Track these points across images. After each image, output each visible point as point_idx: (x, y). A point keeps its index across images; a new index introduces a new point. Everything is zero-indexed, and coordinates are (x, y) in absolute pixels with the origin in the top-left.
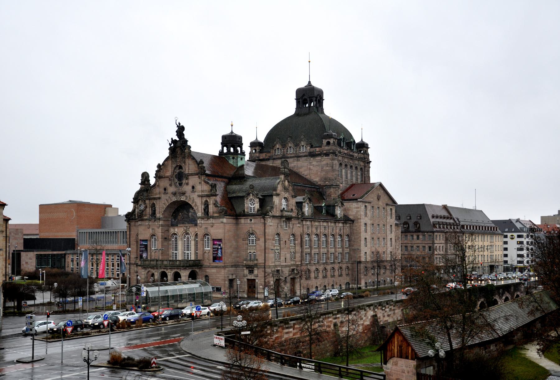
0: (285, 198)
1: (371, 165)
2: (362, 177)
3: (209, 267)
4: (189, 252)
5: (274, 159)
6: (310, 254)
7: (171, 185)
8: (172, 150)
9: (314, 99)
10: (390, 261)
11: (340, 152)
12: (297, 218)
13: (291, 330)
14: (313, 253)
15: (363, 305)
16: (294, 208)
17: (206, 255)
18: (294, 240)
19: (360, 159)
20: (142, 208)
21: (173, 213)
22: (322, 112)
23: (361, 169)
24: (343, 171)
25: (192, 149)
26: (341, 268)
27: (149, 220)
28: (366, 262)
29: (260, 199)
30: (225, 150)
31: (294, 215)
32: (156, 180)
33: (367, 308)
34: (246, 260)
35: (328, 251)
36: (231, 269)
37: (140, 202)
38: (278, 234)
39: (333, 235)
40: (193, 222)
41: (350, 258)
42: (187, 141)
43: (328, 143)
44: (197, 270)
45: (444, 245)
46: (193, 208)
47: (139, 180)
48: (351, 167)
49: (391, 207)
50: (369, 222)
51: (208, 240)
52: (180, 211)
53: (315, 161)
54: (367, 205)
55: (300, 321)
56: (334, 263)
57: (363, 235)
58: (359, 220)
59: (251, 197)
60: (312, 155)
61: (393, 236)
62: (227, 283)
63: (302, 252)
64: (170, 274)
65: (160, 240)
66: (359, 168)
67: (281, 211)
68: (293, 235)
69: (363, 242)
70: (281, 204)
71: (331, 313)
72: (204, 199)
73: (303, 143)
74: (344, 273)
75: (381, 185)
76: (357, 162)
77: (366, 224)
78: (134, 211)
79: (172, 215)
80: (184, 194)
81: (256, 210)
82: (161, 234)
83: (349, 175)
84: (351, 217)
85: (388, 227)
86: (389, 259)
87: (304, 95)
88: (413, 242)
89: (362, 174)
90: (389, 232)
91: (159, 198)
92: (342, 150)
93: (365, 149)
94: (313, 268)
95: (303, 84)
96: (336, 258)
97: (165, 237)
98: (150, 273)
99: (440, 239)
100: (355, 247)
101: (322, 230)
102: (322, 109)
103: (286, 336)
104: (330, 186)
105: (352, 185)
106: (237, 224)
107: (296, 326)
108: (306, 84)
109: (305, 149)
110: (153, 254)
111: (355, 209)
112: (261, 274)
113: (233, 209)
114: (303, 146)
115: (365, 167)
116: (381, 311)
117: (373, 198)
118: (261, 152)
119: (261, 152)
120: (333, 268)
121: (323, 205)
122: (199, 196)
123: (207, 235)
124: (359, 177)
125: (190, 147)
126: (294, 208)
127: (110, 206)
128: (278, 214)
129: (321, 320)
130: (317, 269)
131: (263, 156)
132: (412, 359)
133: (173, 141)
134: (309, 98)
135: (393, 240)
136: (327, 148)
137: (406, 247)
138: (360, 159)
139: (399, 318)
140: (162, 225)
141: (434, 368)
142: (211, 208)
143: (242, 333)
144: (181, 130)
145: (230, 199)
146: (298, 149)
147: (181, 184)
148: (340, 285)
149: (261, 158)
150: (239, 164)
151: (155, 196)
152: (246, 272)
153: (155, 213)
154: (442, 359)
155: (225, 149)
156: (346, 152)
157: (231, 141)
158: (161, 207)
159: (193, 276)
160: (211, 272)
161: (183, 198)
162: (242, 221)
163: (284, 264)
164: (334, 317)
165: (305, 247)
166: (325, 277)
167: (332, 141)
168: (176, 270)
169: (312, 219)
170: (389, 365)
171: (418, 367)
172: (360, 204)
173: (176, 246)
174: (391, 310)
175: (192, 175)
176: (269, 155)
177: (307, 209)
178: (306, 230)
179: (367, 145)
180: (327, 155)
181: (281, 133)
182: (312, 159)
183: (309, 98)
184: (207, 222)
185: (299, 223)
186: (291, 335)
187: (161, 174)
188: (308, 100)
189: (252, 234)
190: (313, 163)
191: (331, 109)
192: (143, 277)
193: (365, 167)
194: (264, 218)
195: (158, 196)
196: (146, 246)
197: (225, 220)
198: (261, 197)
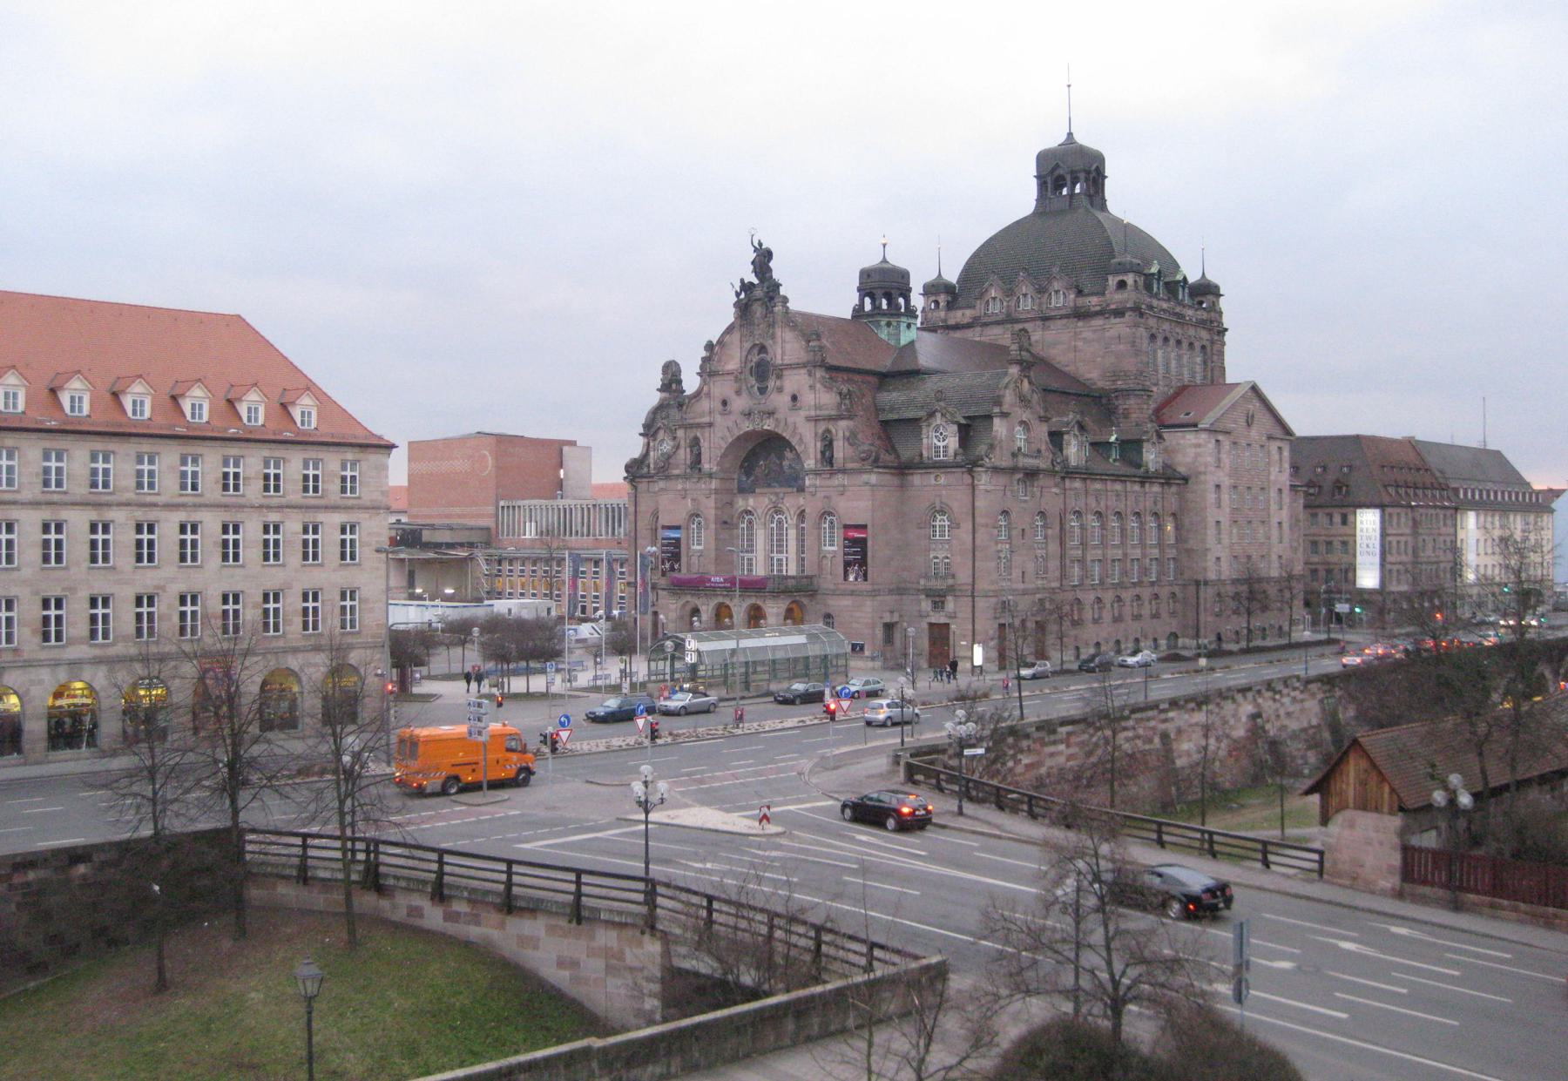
0: (1022, 423)
1: (1228, 337)
2: (1205, 370)
3: (834, 593)
4: (783, 556)
5: (986, 325)
6: (1082, 561)
7: (738, 393)
8: (743, 309)
9: (1082, 176)
10: (1278, 581)
11: (1151, 308)
12: (1051, 473)
13: (1062, 747)
14: (1089, 558)
15: (1229, 689)
16: (1043, 448)
17: (827, 563)
18: (1045, 527)
19: (1202, 323)
20: (667, 447)
21: (745, 460)
22: (1103, 206)
23: (1203, 347)
24: (1160, 353)
25: (792, 306)
26: (1156, 596)
27: (685, 477)
28: (1221, 582)
29: (960, 426)
30: (868, 306)
31: (1042, 464)
32: (704, 382)
33: (1239, 697)
34: (926, 577)
35: (1125, 555)
36: (888, 598)
37: (661, 435)
38: (1005, 513)
39: (1138, 514)
40: (794, 482)
41: (1180, 571)
42: (778, 285)
43: (1122, 285)
44: (805, 601)
45: (1410, 539)
46: (792, 449)
47: (657, 379)
48: (1179, 342)
49: (1279, 443)
50: (1226, 482)
51: (699, 528)
52: (762, 456)
53: (1088, 330)
54: (1220, 438)
55: (1082, 726)
56: (1140, 583)
57: (1212, 515)
58: (1202, 477)
59: (938, 420)
60: (1081, 315)
61: (1284, 515)
62: (879, 632)
63: (1062, 557)
64: (739, 608)
65: (713, 526)
66: (1197, 345)
67: (1014, 455)
68: (1042, 514)
69: (1211, 531)
70: (1012, 439)
71: (1154, 706)
72: (822, 427)
73: (1056, 285)
74: (1164, 609)
75: (1255, 389)
76: (1192, 332)
77: (1218, 486)
78: (646, 455)
79: (741, 466)
80: (771, 414)
81: (951, 452)
82: (713, 512)
83: (1173, 364)
84: (1182, 470)
85: (1273, 494)
86: (1275, 573)
87: (1057, 166)
88: (1333, 532)
89: (1205, 362)
90: (1274, 507)
91: (710, 425)
92: (1155, 302)
93: (1211, 297)
94: (1088, 598)
95: (1054, 140)
96: (1145, 571)
97: (725, 518)
98: (688, 608)
99: (1398, 524)
100: (1192, 544)
101: (1112, 502)
102: (1104, 200)
103: (1049, 762)
104: (1126, 393)
105: (1182, 390)
106: (902, 487)
107: (1073, 739)
108: (1062, 138)
109: (1061, 299)
110: (694, 560)
111: (1190, 449)
112: (965, 612)
113: (892, 449)
114: (1057, 292)
115: (1212, 342)
116: (1270, 703)
117: (1235, 422)
118: (950, 306)
119: (950, 306)
120: (1138, 597)
121: (1113, 439)
122: (808, 419)
123: (830, 514)
124: (1198, 369)
125: (785, 300)
126: (1043, 448)
127: (572, 443)
128: (1006, 462)
129: (1131, 723)
130: (1099, 600)
131: (959, 316)
132: (1391, 813)
133: (746, 287)
134: (1071, 175)
135: (1286, 526)
136: (1119, 296)
137: (1315, 543)
138: (1202, 323)
139: (1314, 722)
140: (717, 491)
141: (1439, 835)
142: (840, 450)
143: (967, 752)
144: (763, 259)
145: (885, 424)
146: (1044, 300)
147: (762, 391)
148: (1155, 640)
149: (951, 322)
150: (903, 342)
151: (698, 420)
152: (926, 605)
153: (699, 462)
154: (1465, 812)
155: (867, 301)
156: (1165, 305)
157: (883, 286)
158: (715, 444)
159: (793, 616)
160: (839, 605)
161: (768, 425)
162: (916, 479)
163: (1021, 586)
164: (1163, 716)
165: (1070, 544)
166: (1118, 619)
167: (1130, 279)
168: (753, 601)
169: (1086, 474)
170: (1335, 828)
171: (1403, 832)
172: (1204, 436)
173: (750, 540)
174: (1294, 700)
175: (790, 367)
176: (968, 312)
177: (1074, 451)
178: (1072, 504)
179: (1217, 287)
180: (1119, 313)
181: (999, 261)
182: (1080, 324)
183: (1071, 175)
184: (829, 482)
185: (1056, 485)
186: (1061, 760)
187: (714, 366)
188: (1068, 178)
189: (942, 512)
190: (1084, 335)
191: (1125, 198)
192: (673, 615)
193: (1212, 342)
194: (970, 472)
195: (706, 419)
196: (862, 543)
197: (873, 478)
198: (963, 421)
